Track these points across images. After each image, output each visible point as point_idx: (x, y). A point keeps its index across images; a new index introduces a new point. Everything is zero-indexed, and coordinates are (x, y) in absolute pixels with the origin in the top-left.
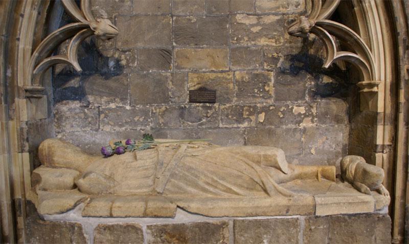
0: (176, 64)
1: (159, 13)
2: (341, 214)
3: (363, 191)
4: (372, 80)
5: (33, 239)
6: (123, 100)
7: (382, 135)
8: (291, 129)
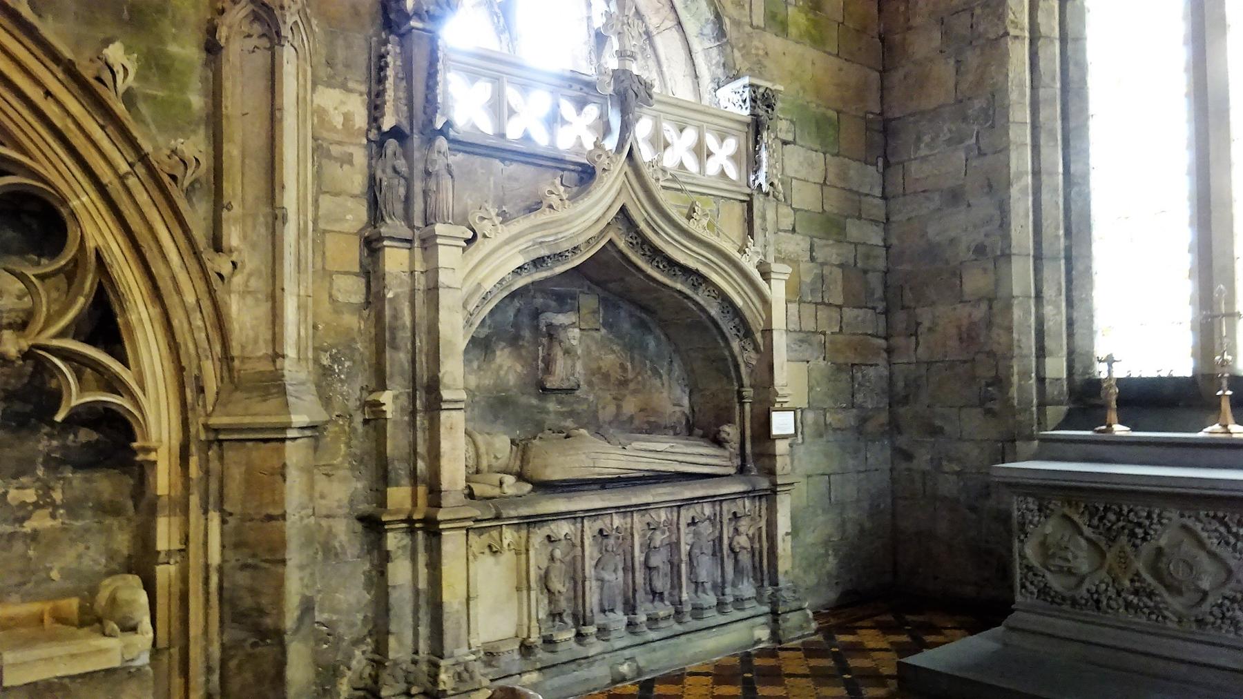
2: (57, 677)
7: (165, 535)
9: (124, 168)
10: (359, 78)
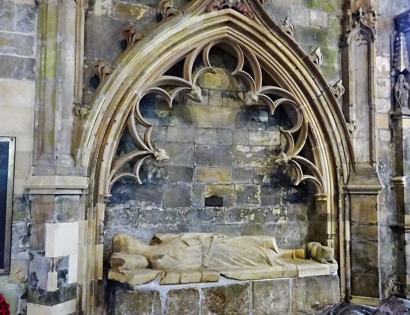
0: (196, 178)
1: (186, 142)
3: (323, 262)
4: (324, 193)
5: (122, 305)
6: (157, 204)
7: (330, 228)
8: (271, 225)
9: (319, 93)
10: (387, 51)
